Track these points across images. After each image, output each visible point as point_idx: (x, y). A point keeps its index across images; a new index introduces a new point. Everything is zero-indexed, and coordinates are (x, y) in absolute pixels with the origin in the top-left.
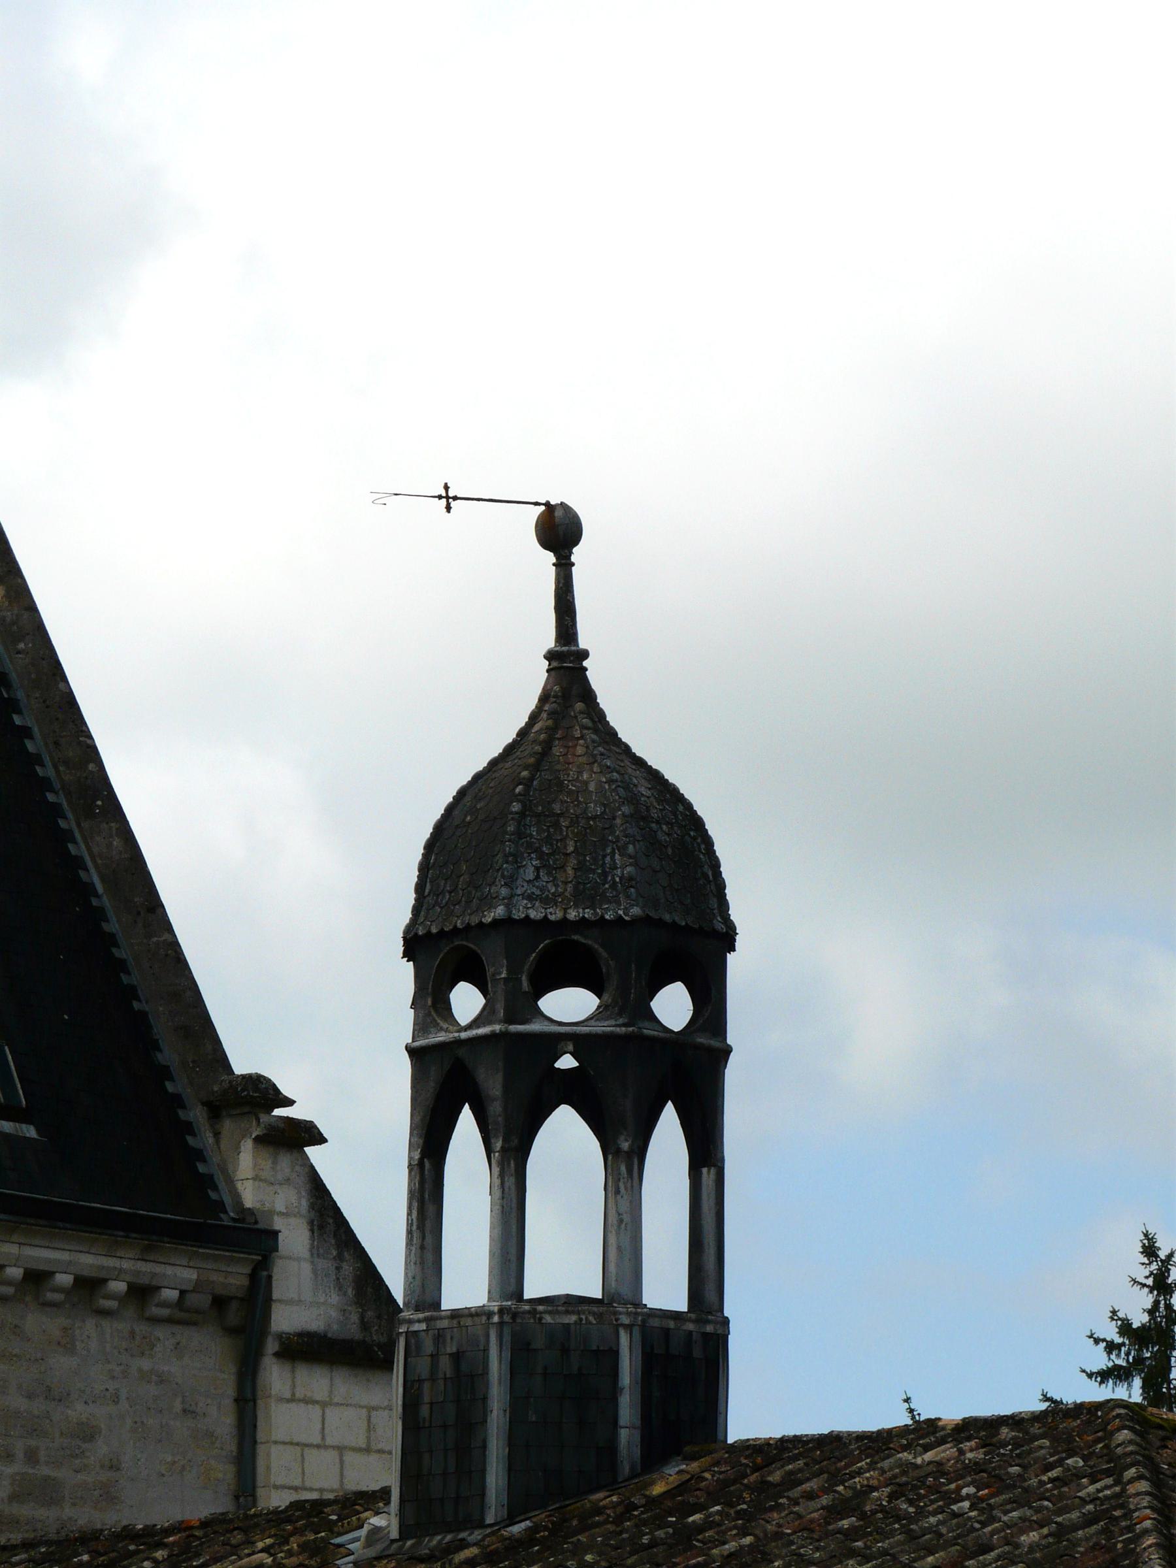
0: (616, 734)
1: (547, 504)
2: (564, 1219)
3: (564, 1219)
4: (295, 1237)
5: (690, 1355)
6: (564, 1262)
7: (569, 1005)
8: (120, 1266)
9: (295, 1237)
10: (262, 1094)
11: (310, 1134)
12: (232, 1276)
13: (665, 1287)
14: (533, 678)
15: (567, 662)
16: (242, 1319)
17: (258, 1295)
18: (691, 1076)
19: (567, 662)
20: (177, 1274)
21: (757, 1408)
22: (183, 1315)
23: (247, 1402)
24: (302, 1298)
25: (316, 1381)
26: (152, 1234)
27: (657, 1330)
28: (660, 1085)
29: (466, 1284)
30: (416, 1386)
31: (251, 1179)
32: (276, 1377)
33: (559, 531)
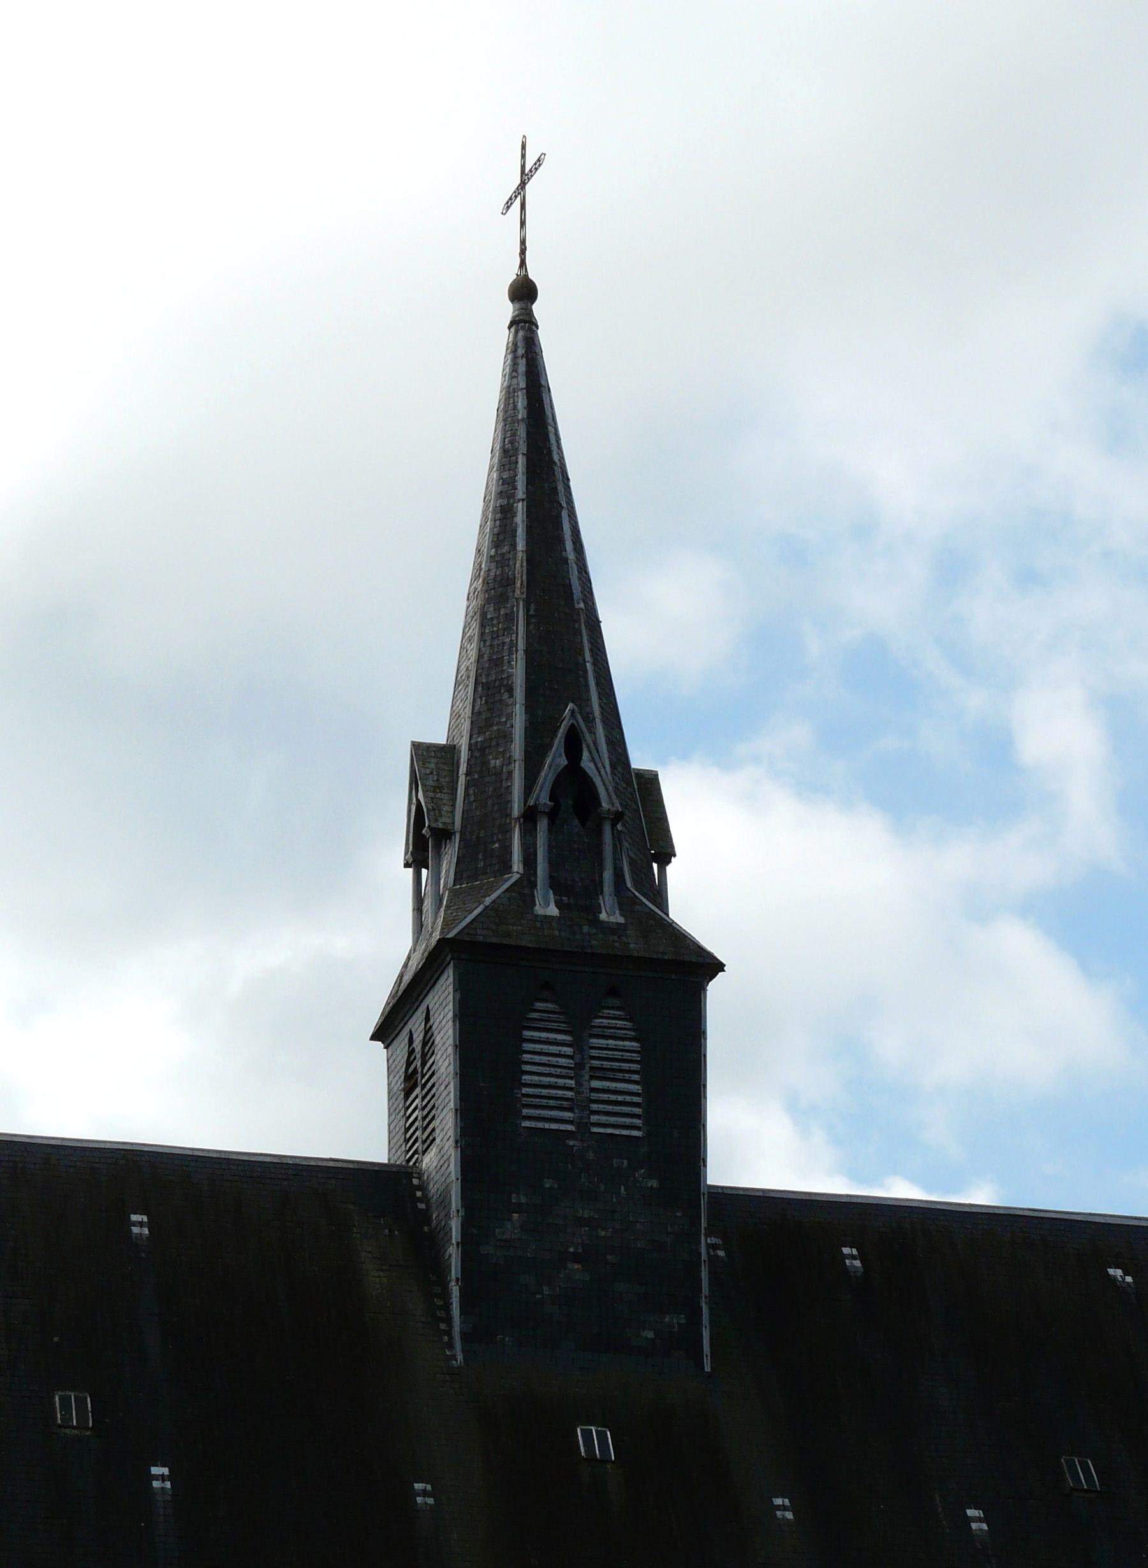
0: (666, 854)
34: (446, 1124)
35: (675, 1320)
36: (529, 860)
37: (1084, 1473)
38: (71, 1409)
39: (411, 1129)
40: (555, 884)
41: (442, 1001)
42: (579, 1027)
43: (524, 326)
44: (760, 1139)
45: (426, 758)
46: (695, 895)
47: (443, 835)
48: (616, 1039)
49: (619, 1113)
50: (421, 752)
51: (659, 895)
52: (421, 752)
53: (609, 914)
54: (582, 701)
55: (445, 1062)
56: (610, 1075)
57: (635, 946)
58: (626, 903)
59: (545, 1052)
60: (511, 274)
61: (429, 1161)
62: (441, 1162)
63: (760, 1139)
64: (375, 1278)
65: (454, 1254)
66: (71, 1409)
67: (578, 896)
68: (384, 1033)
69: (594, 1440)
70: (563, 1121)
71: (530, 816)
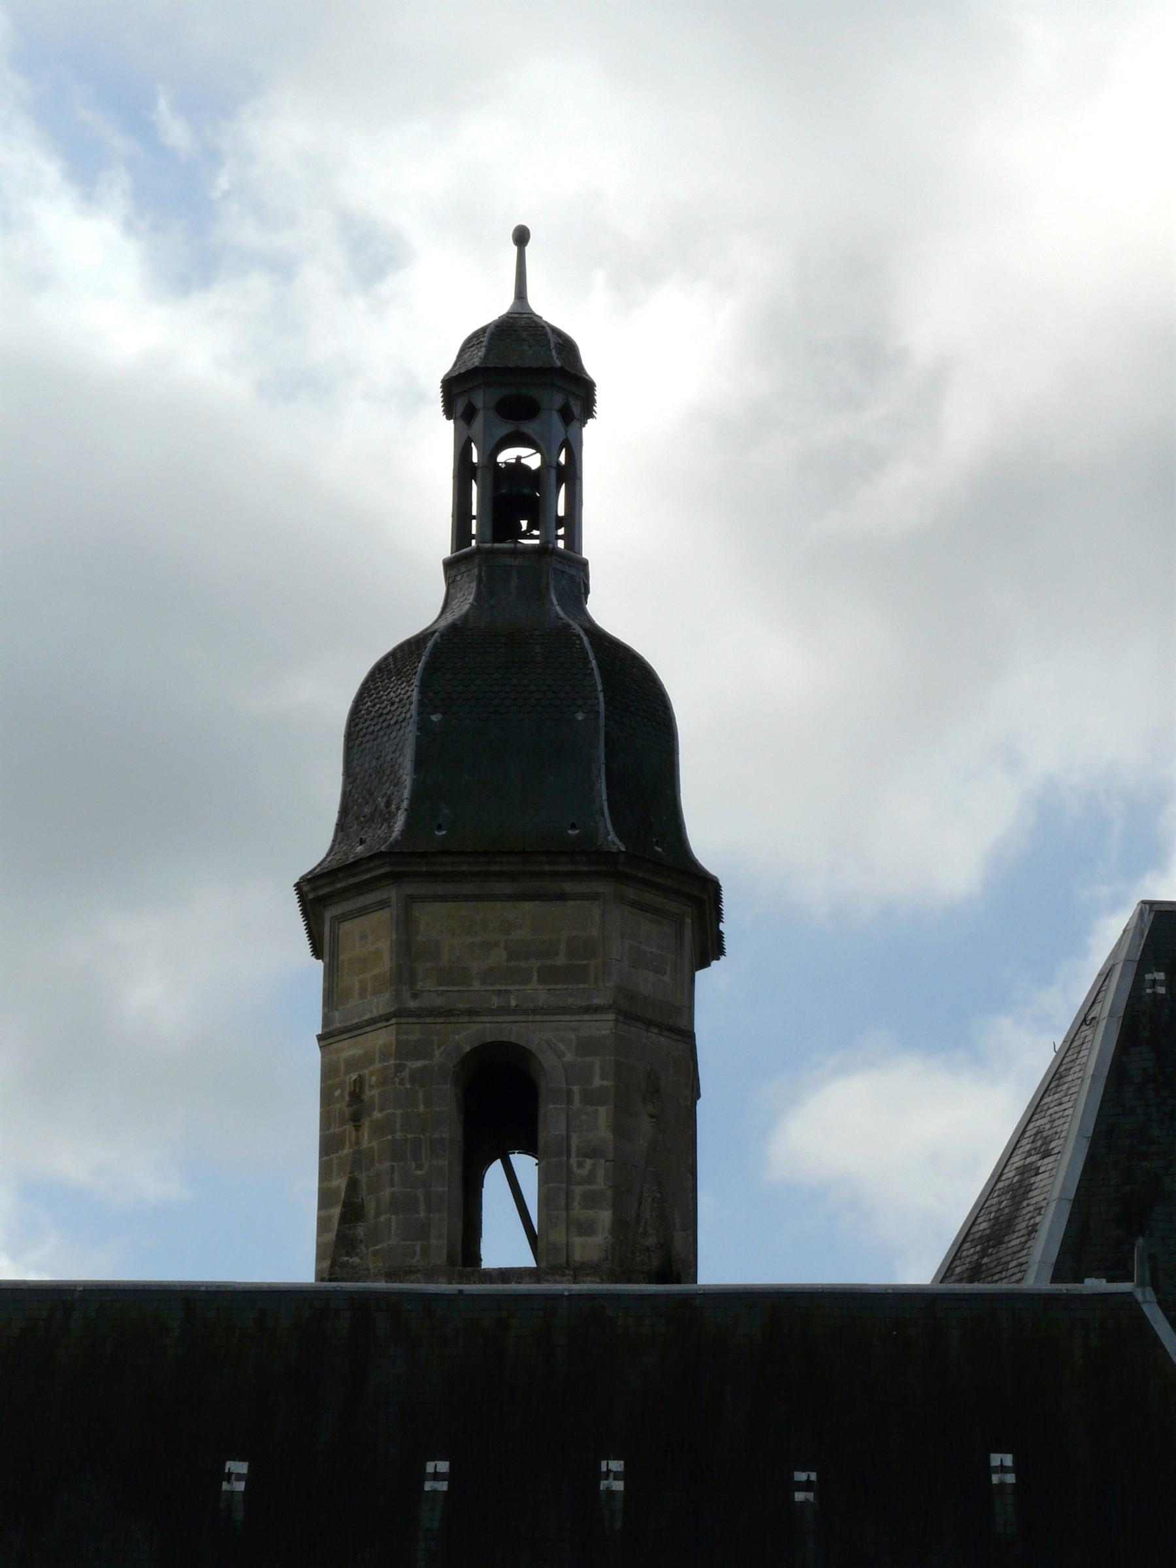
33: (521, 237)
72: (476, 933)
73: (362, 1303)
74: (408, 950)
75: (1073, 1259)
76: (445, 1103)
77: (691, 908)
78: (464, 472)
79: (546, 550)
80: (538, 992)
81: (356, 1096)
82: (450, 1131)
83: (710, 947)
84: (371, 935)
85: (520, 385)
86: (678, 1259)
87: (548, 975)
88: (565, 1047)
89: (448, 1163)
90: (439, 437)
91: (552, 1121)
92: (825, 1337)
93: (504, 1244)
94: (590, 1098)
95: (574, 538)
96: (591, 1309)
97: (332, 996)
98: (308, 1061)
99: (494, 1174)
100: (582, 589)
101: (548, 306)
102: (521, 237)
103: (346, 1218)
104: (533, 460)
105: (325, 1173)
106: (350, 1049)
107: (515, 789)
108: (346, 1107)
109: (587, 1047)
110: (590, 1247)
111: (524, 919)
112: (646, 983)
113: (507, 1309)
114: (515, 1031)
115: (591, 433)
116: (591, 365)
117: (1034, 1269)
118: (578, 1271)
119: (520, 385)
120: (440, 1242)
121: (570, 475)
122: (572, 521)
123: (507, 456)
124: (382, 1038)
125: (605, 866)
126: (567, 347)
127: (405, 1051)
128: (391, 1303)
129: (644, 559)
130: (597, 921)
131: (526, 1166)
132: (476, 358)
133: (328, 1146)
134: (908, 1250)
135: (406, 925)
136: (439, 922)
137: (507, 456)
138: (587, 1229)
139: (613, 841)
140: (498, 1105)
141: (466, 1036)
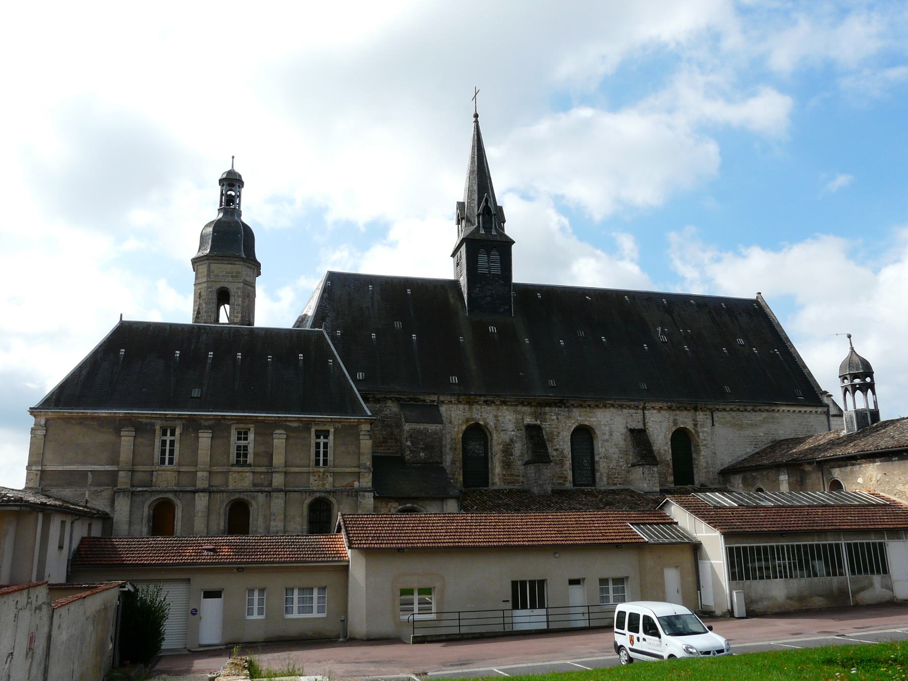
0: (504, 222)
1: (878, 412)
2: (860, 401)
3: (860, 401)
4: (831, 405)
5: (875, 414)
6: (861, 405)
7: (857, 381)
8: (814, 409)
9: (831, 405)
10: (826, 392)
11: (831, 396)
12: (825, 409)
13: (872, 407)
14: (849, 351)
15: (852, 348)
16: (827, 413)
17: (828, 411)
18: (871, 386)
19: (852, 348)
20: (820, 410)
21: (883, 417)
22: (821, 413)
23: (829, 421)
24: (833, 411)
25: (835, 418)
26: (817, 406)
27: (872, 412)
28: (868, 387)
29: (850, 407)
30: (854, 357)
31: (825, 400)
32: (831, 418)
33: (849, 337)
34: (464, 272)
35: (89, 474)
36: (479, 223)
37: (582, 334)
38: (398, 325)
39: (458, 274)
40: (484, 227)
41: (463, 249)
42: (489, 255)
43: (476, 122)
44: (520, 276)
45: (461, 205)
46: (509, 230)
47: (463, 219)
48: (495, 256)
49: (496, 269)
50: (458, 203)
51: (503, 229)
52: (458, 203)
53: (494, 233)
54: (488, 193)
55: (464, 261)
56: (182, 570)
57: (499, 239)
58: (497, 231)
59: (482, 259)
60: (474, 113)
61: (461, 279)
62: (463, 281)
63: (520, 276)
64: (452, 301)
65: (465, 296)
66: (398, 325)
67: (488, 229)
68: (453, 255)
69: (492, 329)
70: (486, 271)
71: (479, 215)
72: (222, 269)
73: (199, 327)
74: (209, 271)
75: (314, 325)
76: (215, 296)
77: (256, 267)
78: (222, 194)
79: (235, 209)
80: (230, 279)
81: (200, 294)
82: (215, 301)
83: (259, 274)
84: (203, 268)
85: (232, 182)
86: (251, 323)
87: (232, 277)
88: (234, 288)
89: (215, 305)
90: (218, 188)
91: (232, 300)
92: (272, 336)
93: (223, 319)
94: (238, 297)
95: (239, 207)
96: (237, 330)
97: (196, 278)
98: (192, 288)
99: (222, 308)
100: (240, 215)
101: (237, 169)
102: (849, 337)
103: (198, 314)
104: (233, 194)
105: (194, 306)
106: (199, 287)
107: (230, 246)
108: (198, 296)
109: (238, 288)
110: (238, 320)
111: (229, 267)
112: (248, 279)
113: (222, 332)
114: (226, 285)
115: (243, 190)
116: (244, 179)
117: (308, 327)
118: (235, 324)
119: (232, 182)
120: (213, 318)
121: (239, 196)
122: (239, 204)
123: (229, 193)
124: (205, 285)
125: (243, 260)
126: (240, 176)
127: (208, 287)
128: (204, 327)
129: (251, 212)
130: (239, 267)
131: (227, 307)
132: (225, 176)
133: (195, 302)
134: (287, 322)
135: (209, 267)
136: (214, 267)
137: (229, 193)
138: (237, 317)
139: (244, 256)
140: (223, 297)
141: (218, 286)
